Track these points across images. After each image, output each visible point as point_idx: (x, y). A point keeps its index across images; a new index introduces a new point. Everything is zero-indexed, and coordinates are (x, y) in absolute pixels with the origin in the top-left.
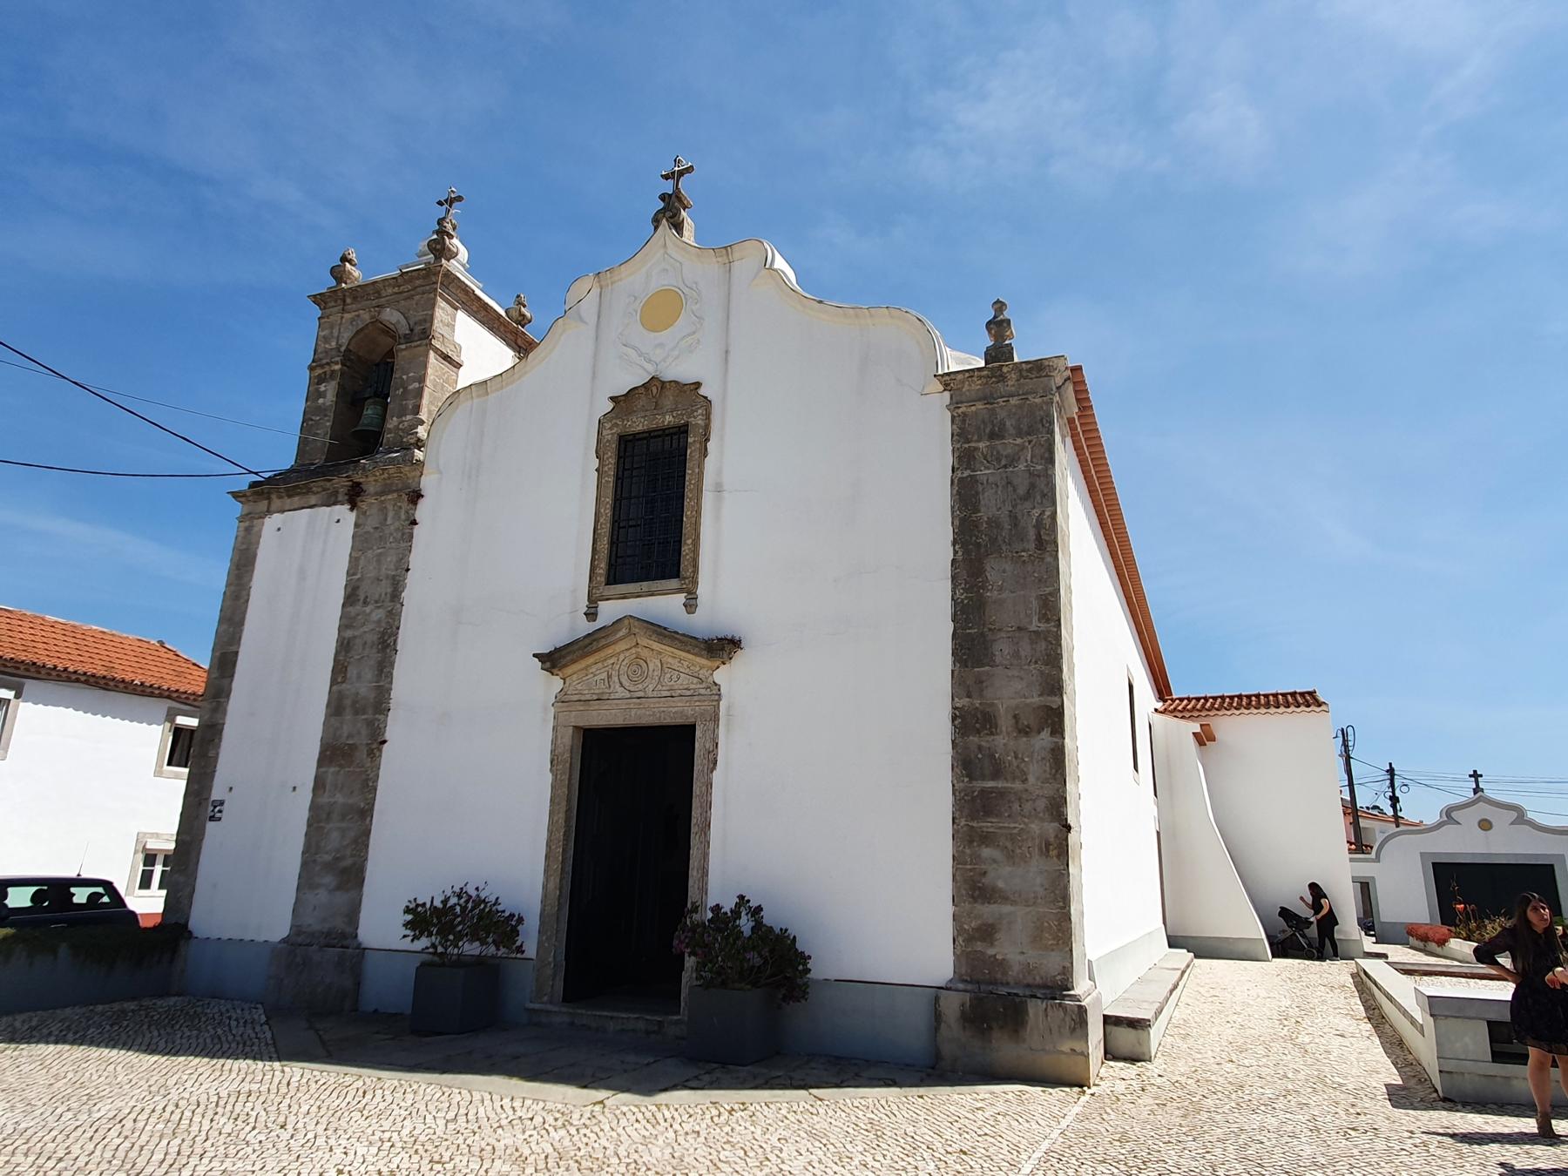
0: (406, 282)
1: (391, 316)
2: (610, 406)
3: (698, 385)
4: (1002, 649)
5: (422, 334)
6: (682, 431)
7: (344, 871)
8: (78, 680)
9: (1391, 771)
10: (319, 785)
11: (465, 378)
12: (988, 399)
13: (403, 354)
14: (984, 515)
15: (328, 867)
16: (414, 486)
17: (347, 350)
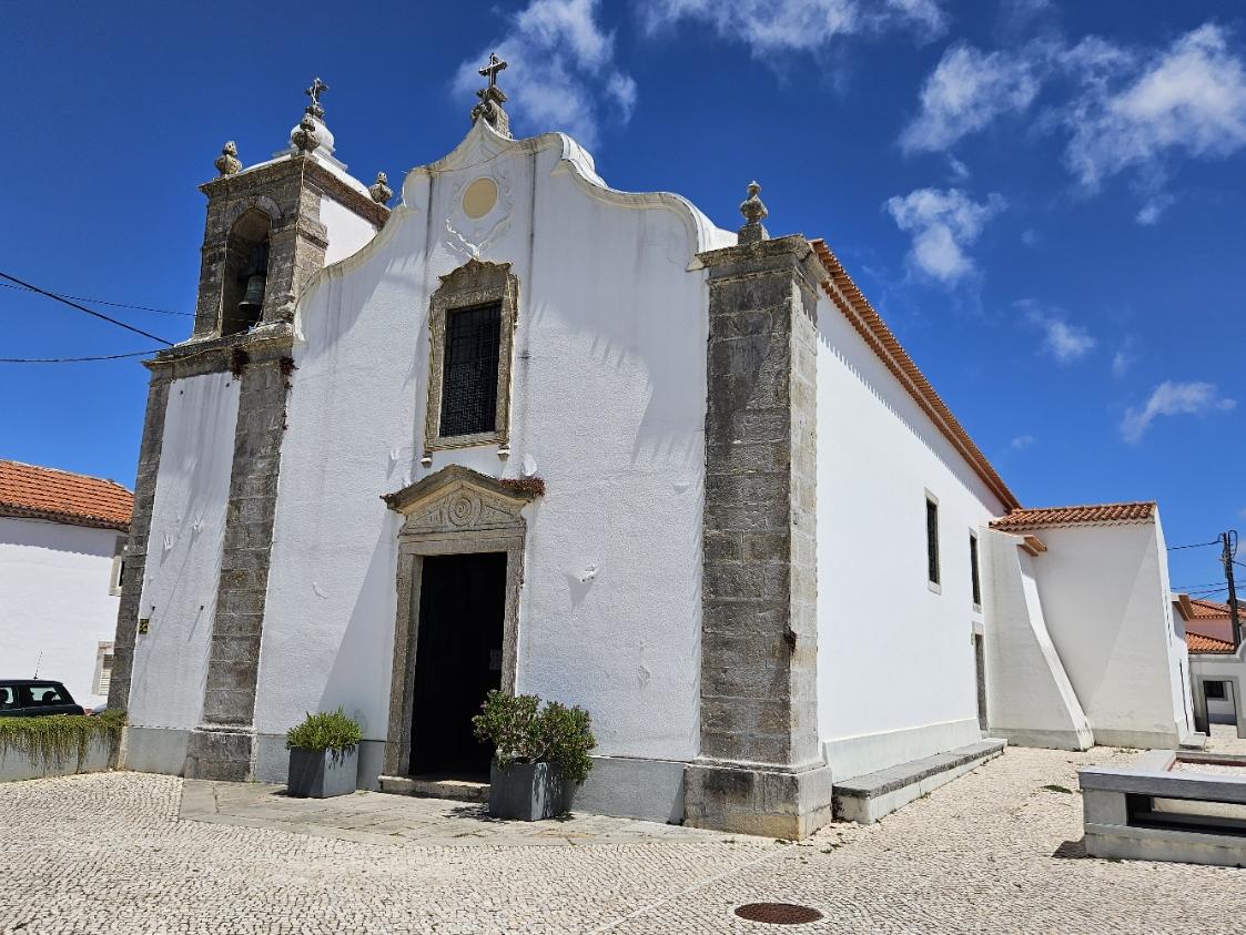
0: (276, 172)
1: (265, 202)
3: (508, 266)
4: (744, 487)
5: (290, 215)
6: (498, 304)
7: (242, 673)
8: (40, 517)
10: (221, 604)
11: (331, 257)
12: (739, 274)
13: (276, 236)
14: (732, 375)
15: (230, 670)
17: (232, 234)
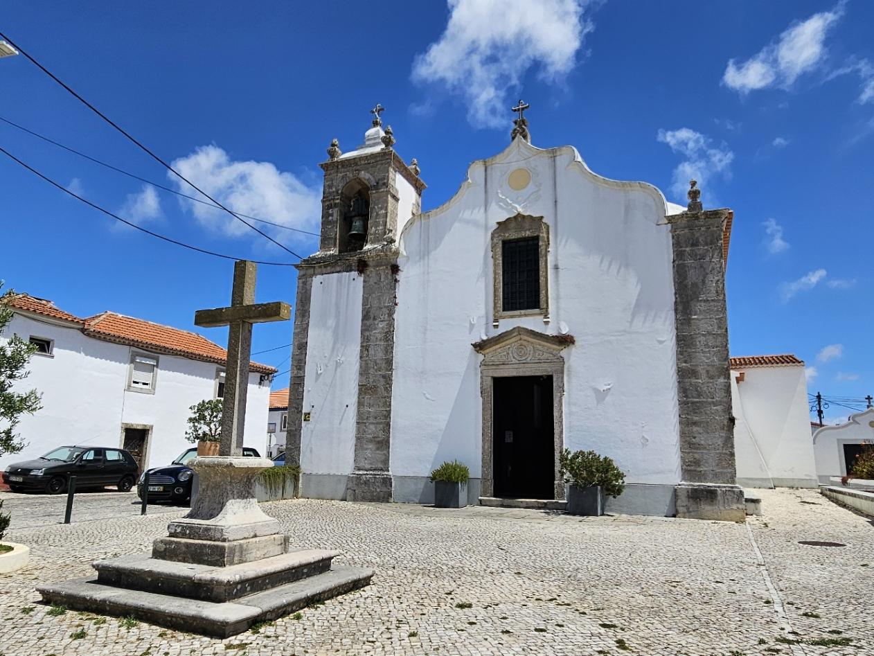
1: (364, 175)
2: (497, 226)
6: (537, 238)
8: (180, 355)
9: (819, 397)
12: (691, 228)
13: (373, 195)
14: (689, 282)
16: (393, 263)
17: (342, 192)
